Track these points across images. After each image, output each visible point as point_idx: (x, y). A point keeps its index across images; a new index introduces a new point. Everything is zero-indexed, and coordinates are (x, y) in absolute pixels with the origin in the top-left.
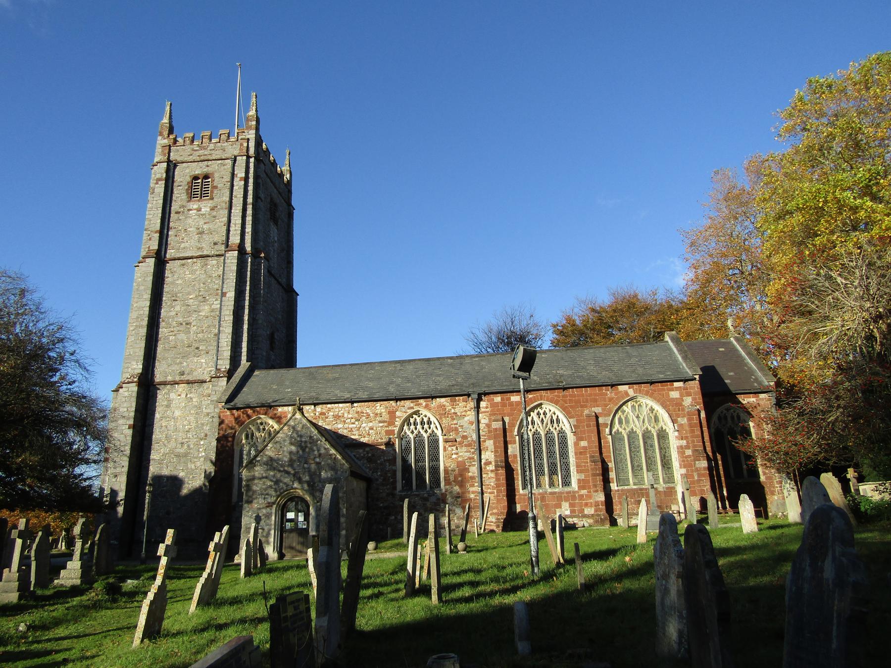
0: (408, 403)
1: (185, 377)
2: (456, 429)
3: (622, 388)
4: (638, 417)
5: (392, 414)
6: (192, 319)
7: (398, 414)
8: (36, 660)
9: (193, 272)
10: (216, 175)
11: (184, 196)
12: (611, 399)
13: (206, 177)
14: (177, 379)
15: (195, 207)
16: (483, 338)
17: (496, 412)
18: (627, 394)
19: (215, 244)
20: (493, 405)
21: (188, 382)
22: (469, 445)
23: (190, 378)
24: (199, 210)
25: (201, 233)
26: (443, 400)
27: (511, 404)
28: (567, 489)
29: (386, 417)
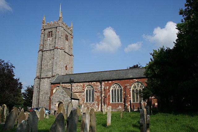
0: (87, 83)
1: (47, 77)
2: (97, 89)
3: (134, 80)
4: (138, 86)
5: (84, 85)
6: (48, 64)
7: (85, 85)
8: (110, 118)
9: (48, 54)
10: (53, 31)
11: (47, 37)
12: (132, 82)
13: (51, 32)
14: (45, 77)
15: (49, 39)
16: (166, 48)
17: (105, 86)
18: (135, 81)
19: (53, 47)
20: (105, 83)
21: (47, 78)
22: (99, 93)
23: (48, 77)
24: (50, 39)
25: (50, 45)
26: (95, 82)
27: (109, 83)
28: (121, 102)
29: (83, 86)
